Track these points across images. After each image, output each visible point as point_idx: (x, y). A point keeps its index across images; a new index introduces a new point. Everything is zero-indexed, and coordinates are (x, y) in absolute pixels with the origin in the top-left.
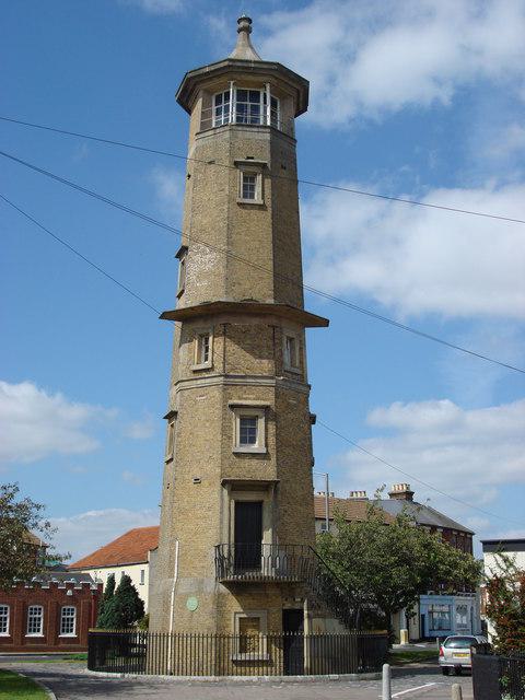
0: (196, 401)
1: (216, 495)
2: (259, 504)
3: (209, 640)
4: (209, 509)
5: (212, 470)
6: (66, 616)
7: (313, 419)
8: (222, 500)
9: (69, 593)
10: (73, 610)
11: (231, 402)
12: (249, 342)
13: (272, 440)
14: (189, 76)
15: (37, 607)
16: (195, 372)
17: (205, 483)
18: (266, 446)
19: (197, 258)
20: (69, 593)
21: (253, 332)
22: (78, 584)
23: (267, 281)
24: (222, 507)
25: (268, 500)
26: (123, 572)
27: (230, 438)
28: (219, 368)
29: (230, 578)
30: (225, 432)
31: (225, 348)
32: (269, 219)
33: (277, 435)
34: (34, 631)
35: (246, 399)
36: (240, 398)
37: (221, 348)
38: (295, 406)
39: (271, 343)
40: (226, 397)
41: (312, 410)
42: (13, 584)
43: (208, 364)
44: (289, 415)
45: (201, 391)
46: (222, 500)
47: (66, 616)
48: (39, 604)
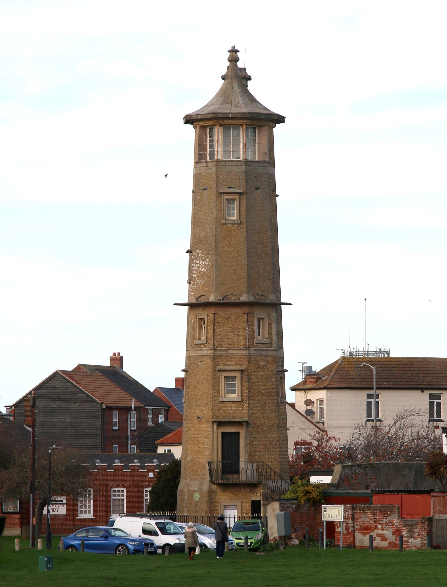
0: (198, 365)
1: (210, 429)
2: (238, 434)
3: (206, 519)
4: (206, 437)
6: (116, 498)
8: (213, 432)
10: (122, 491)
11: (218, 368)
12: (230, 325)
13: (245, 392)
18: (242, 396)
21: (233, 318)
24: (213, 437)
25: (242, 432)
26: (293, 389)
27: (218, 391)
31: (214, 330)
32: (244, 234)
33: (248, 389)
34: (85, 512)
35: (228, 365)
36: (225, 365)
37: (212, 329)
38: (264, 366)
39: (245, 325)
42: (96, 467)
44: (260, 373)
46: (213, 432)
48: (122, 487)
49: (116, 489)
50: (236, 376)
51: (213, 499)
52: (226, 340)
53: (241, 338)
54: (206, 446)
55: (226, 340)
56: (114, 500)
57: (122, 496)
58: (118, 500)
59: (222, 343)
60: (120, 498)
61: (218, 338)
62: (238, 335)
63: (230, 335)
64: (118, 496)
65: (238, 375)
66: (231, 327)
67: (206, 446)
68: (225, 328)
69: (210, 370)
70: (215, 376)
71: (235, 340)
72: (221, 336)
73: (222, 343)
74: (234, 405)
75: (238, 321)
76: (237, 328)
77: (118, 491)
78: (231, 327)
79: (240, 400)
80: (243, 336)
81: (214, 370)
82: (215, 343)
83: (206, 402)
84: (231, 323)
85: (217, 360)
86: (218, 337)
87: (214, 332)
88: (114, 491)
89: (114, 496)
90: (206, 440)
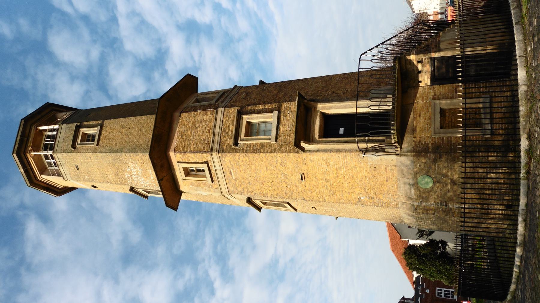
0: (236, 179)
5: (292, 159)
6: (443, 295)
7: (262, 82)
9: (427, 291)
10: (438, 290)
12: (189, 132)
14: (29, 185)
15: (437, 291)
16: (213, 181)
17: (304, 169)
19: (135, 178)
20: (427, 291)
22: (422, 285)
23: (251, 158)
24: (326, 151)
28: (206, 157)
29: (394, 139)
30: (257, 149)
31: (191, 152)
37: (192, 155)
40: (229, 150)
41: (258, 83)
43: (205, 167)
45: (227, 174)
47: (443, 295)
49: (437, 294)
50: (247, 122)
51: (428, 148)
52: (204, 137)
53: (205, 118)
54: (341, 164)
55: (204, 137)
56: (445, 296)
57: (441, 290)
58: (445, 294)
59: (206, 142)
60: (443, 292)
61: (200, 147)
62: (201, 122)
63: (200, 132)
64: (441, 293)
65: (246, 118)
66: (191, 132)
67: (341, 164)
68: (191, 138)
69: (237, 158)
70: (243, 149)
71: (205, 126)
72: (198, 143)
73: (206, 142)
74: (283, 123)
75: (186, 123)
76: (193, 124)
77: (438, 293)
78: (191, 132)
79: (277, 112)
80: (203, 115)
81: (237, 151)
82: (205, 150)
83: (279, 164)
84: (187, 131)
85: (225, 147)
86: (199, 147)
87: (194, 152)
88: (438, 295)
89: (441, 296)
90: (331, 163)
